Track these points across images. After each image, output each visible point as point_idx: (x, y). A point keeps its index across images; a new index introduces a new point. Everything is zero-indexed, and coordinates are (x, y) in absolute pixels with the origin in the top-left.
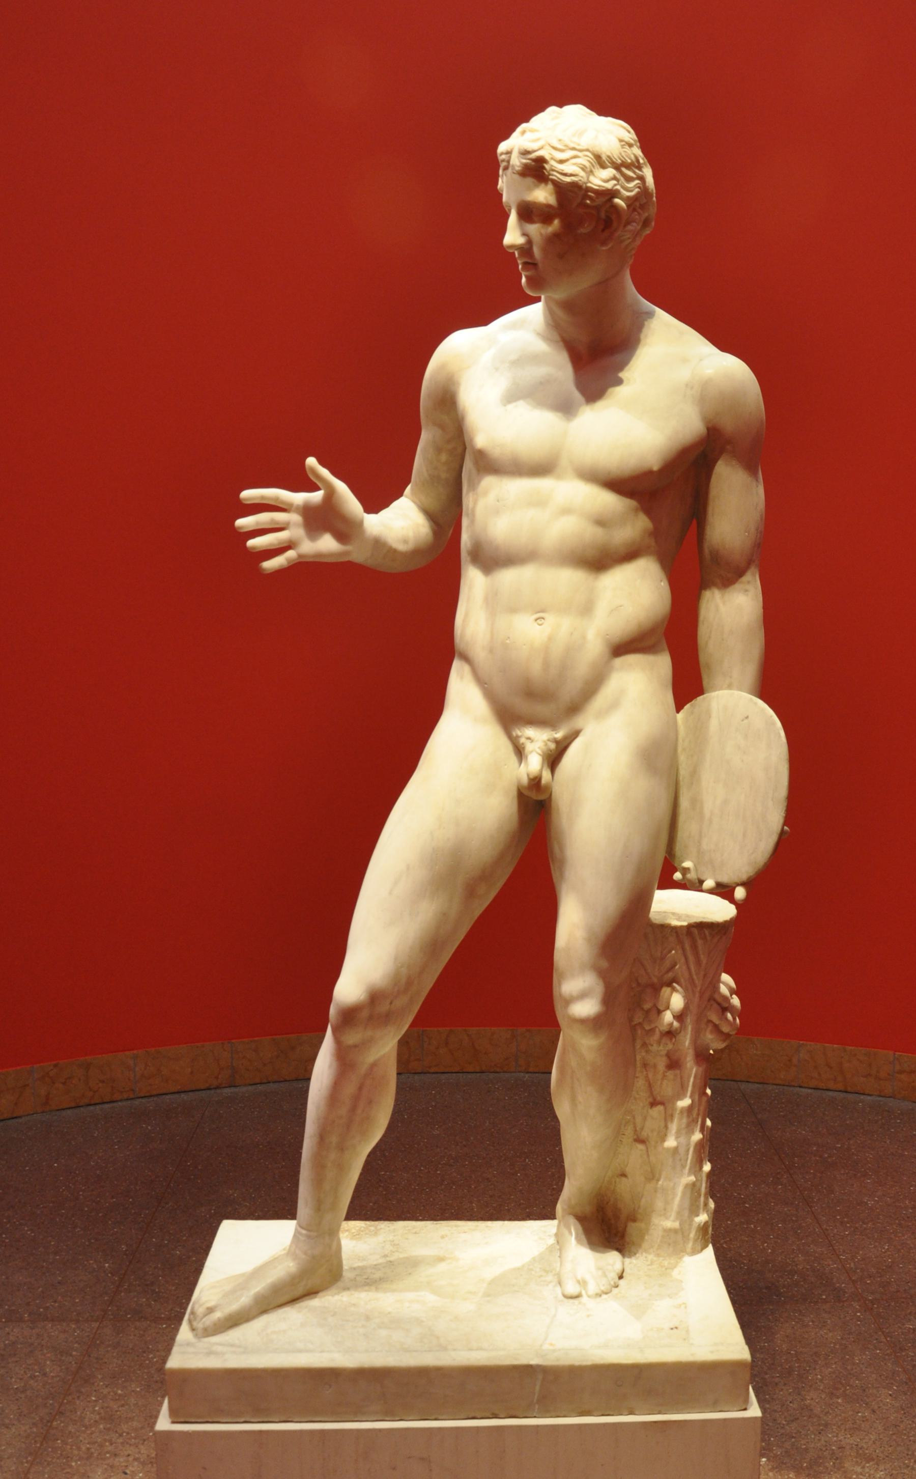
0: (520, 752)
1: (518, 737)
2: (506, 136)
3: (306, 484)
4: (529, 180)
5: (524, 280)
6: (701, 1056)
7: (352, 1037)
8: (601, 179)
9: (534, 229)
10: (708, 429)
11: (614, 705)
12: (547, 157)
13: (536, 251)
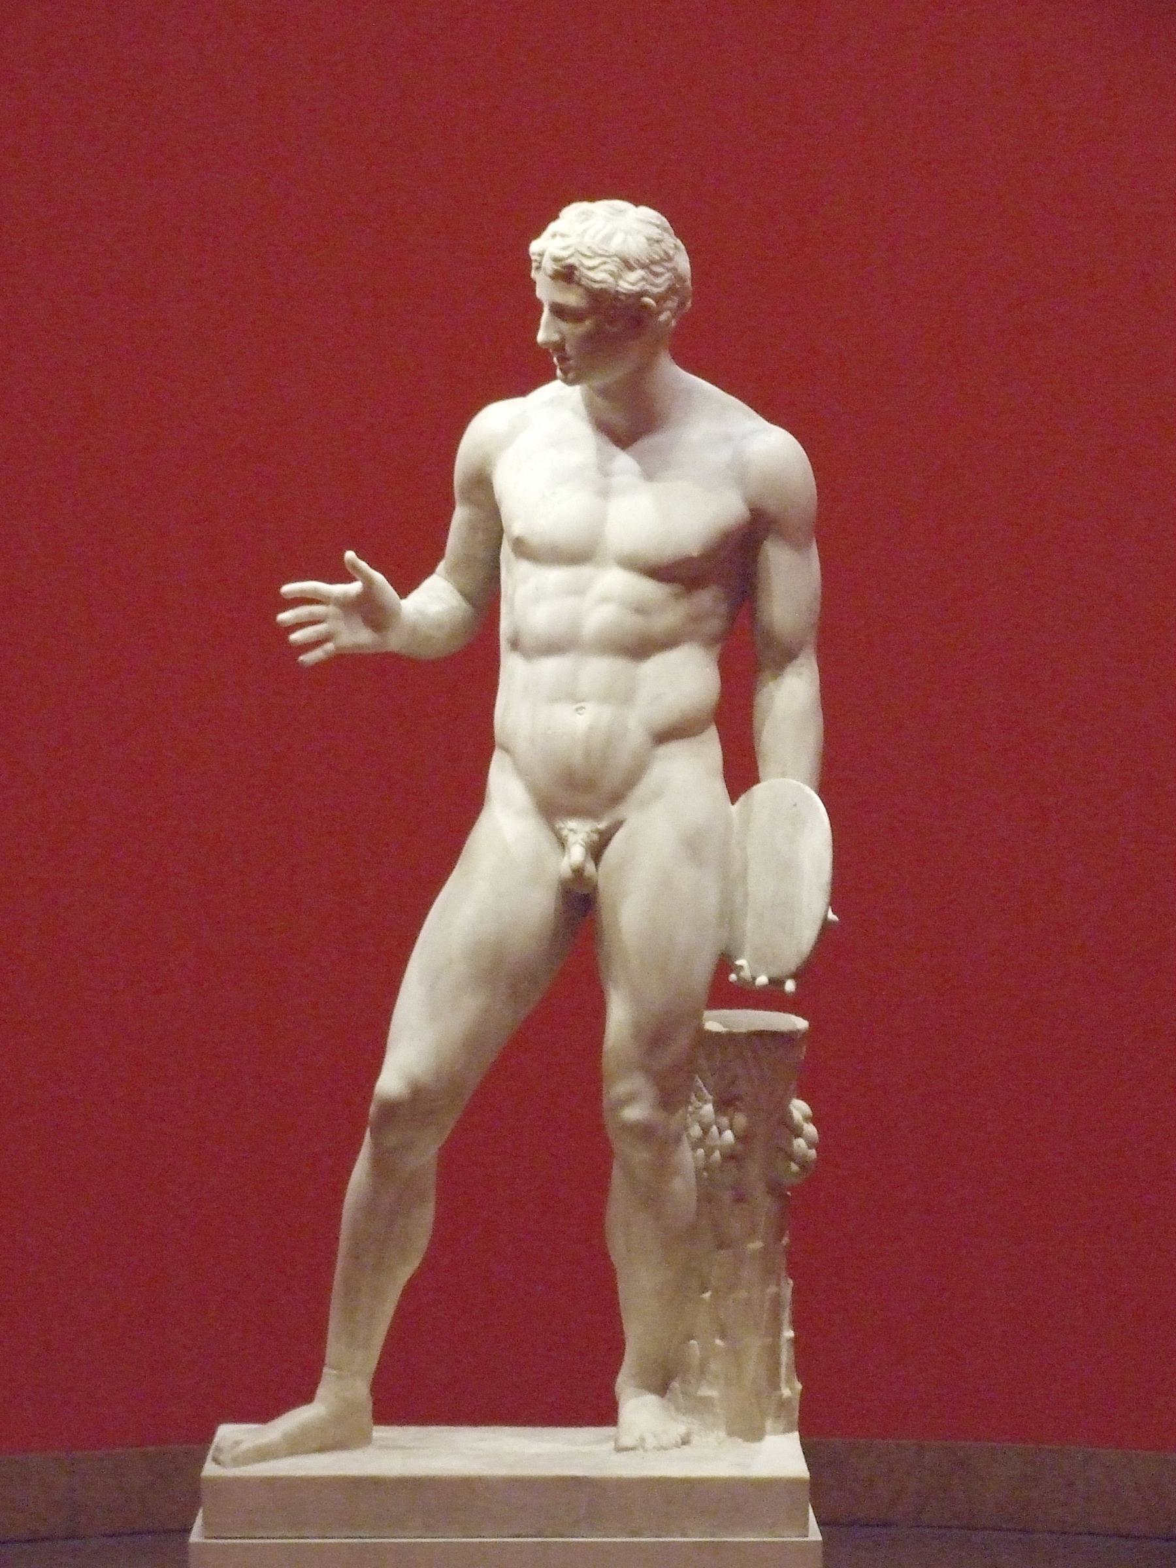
0: (562, 843)
1: (561, 829)
2: (537, 234)
3: (344, 575)
4: (562, 284)
5: (555, 359)
6: (775, 1189)
7: (392, 1139)
8: (630, 282)
9: (565, 327)
10: (751, 510)
11: (657, 795)
12: (577, 264)
13: (568, 348)
